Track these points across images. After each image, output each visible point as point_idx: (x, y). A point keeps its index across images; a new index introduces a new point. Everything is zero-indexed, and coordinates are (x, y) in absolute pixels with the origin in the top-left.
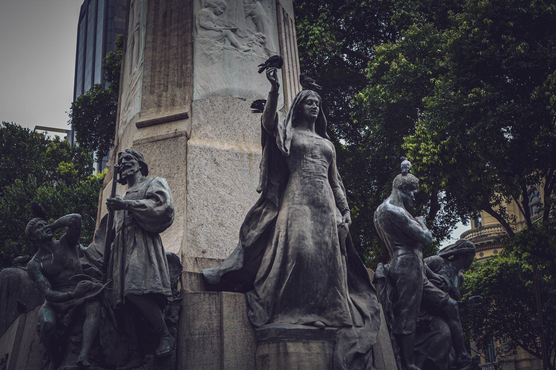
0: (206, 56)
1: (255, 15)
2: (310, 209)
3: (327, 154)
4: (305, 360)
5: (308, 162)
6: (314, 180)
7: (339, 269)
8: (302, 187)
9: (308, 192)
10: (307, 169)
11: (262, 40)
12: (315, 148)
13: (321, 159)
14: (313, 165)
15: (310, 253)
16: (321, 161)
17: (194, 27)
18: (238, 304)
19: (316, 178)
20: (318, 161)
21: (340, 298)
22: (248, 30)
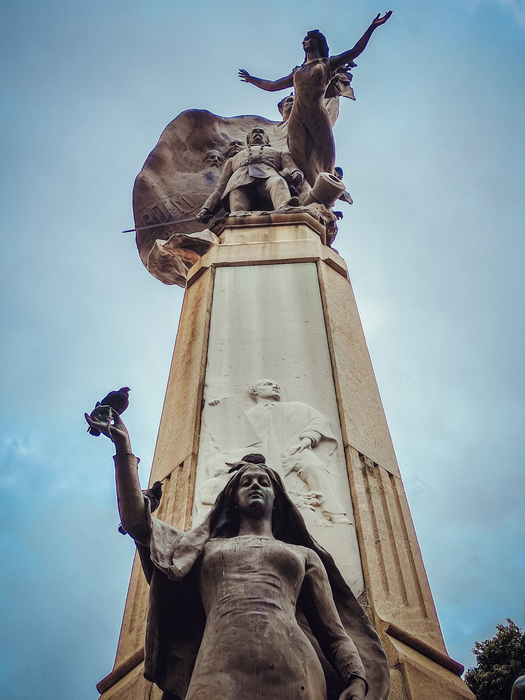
1: (300, 468)
2: (234, 677)
3: (276, 559)
5: (230, 582)
6: (243, 614)
8: (217, 635)
9: (228, 644)
10: (228, 597)
11: (315, 500)
12: (250, 554)
14: (241, 585)
16: (261, 574)
17: (194, 508)
19: (247, 610)
20: (254, 577)
22: (290, 493)
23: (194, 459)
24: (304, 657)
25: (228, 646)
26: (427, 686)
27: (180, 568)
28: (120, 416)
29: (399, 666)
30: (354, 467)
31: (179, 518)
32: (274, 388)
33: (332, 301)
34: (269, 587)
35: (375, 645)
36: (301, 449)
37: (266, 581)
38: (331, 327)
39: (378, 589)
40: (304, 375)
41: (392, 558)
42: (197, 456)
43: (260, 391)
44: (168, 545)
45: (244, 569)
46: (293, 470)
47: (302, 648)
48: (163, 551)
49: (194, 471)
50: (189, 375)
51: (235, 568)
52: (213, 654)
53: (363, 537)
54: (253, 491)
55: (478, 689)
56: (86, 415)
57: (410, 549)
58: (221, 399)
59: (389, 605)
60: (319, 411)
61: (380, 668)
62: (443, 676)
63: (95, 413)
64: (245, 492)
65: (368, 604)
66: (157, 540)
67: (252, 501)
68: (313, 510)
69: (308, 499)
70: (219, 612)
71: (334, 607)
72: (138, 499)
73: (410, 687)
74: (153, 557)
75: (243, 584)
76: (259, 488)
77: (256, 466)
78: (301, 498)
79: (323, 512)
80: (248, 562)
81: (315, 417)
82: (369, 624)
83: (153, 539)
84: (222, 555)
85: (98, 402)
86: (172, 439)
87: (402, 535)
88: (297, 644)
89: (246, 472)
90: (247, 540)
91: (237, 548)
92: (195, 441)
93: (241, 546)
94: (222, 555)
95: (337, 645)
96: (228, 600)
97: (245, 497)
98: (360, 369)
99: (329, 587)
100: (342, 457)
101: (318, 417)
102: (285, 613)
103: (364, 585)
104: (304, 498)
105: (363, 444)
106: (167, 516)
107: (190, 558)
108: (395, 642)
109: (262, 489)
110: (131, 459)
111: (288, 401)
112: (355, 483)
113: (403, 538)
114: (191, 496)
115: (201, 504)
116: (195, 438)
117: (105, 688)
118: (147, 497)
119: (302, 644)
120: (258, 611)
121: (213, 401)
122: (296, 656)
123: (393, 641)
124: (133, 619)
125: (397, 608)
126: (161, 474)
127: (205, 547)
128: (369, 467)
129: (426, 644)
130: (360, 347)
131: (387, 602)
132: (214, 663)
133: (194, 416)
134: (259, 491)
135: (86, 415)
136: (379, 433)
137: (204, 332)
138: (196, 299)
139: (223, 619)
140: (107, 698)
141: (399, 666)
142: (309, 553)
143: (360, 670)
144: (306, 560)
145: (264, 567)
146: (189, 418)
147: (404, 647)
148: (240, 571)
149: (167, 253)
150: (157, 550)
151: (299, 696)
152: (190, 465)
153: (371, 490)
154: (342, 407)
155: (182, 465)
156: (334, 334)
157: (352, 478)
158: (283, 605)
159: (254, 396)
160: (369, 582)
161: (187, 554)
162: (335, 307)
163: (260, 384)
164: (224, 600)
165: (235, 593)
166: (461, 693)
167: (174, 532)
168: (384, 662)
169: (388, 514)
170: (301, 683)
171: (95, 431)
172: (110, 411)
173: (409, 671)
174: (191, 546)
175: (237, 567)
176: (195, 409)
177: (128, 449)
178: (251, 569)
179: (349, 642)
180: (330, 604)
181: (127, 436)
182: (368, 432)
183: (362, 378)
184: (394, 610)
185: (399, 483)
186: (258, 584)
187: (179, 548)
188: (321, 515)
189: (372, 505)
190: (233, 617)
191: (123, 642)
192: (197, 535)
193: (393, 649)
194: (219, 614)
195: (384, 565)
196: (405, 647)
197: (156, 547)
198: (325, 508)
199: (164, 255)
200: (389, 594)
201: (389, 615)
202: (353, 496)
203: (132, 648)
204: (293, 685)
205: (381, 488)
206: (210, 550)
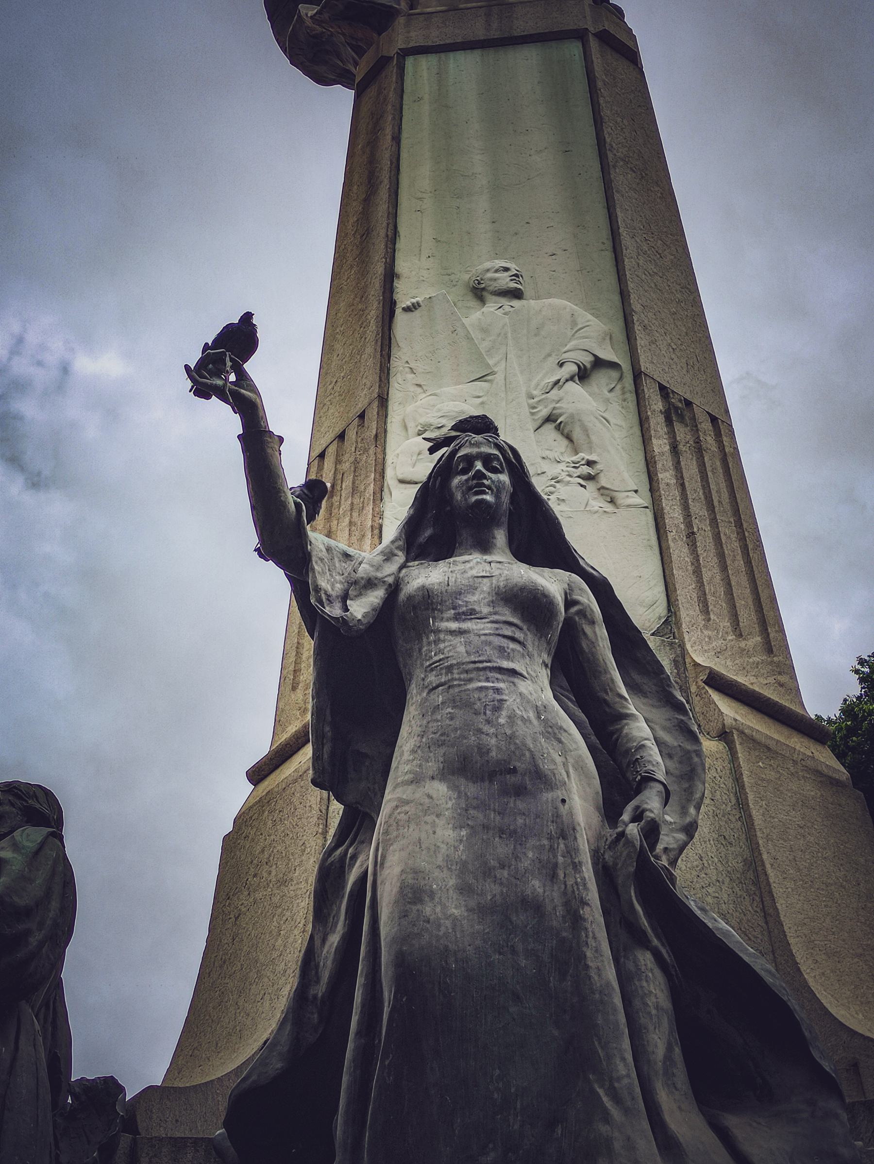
1: (561, 415)
2: (454, 788)
3: (515, 596)
5: (442, 636)
7: (597, 996)
8: (425, 722)
10: (440, 660)
11: (586, 470)
12: (472, 588)
13: (496, 617)
14: (458, 641)
15: (452, 947)
17: (386, 489)
19: (470, 680)
20: (481, 626)
21: (606, 1118)
22: (544, 458)
24: (564, 752)
25: (443, 738)
26: (771, 765)
27: (359, 617)
28: (244, 366)
29: (724, 735)
30: (650, 409)
31: (361, 505)
33: (611, 111)
34: (504, 642)
35: (682, 720)
36: (561, 383)
37: (500, 632)
38: (610, 159)
39: (691, 613)
40: (565, 250)
41: (715, 560)
42: (387, 400)
43: (488, 282)
44: (338, 578)
45: (463, 613)
47: (562, 738)
48: (330, 589)
49: (383, 426)
50: (367, 256)
51: (449, 612)
52: (419, 752)
53: (666, 528)
54: (475, 482)
55: (861, 729)
56: (187, 367)
57: (745, 542)
59: (710, 638)
60: (591, 314)
61: (690, 759)
62: (797, 748)
63: (202, 364)
64: (462, 484)
65: (674, 638)
67: (474, 498)
68: (582, 486)
70: (426, 683)
71: (613, 667)
72: (284, 505)
73: (743, 768)
74: (314, 599)
75: (462, 639)
76: (484, 477)
77: (478, 438)
78: (562, 466)
79: (599, 489)
80: (470, 602)
81: (584, 325)
82: (671, 687)
83: (313, 569)
84: (428, 591)
85: (206, 344)
86: (345, 371)
87: (732, 520)
88: (553, 732)
89: (462, 449)
90: (468, 565)
91: (452, 580)
92: (382, 374)
93: (458, 576)
94: (428, 591)
95: (618, 727)
96: (440, 665)
97: (463, 492)
98: (660, 234)
99: (605, 635)
101: (588, 326)
102: (533, 682)
103: (668, 607)
104: (567, 467)
105: (667, 370)
106: (342, 503)
107: (375, 597)
108: (719, 698)
109: (491, 478)
110: (269, 439)
111: (538, 298)
112: (653, 438)
113: (733, 525)
114: (379, 468)
115: (398, 482)
116: (381, 369)
117: (259, 777)
118: (299, 500)
119: (562, 732)
120: (489, 681)
121: (409, 303)
122: (552, 751)
123: (715, 696)
124: (297, 668)
125: (723, 642)
126: (329, 432)
127: (399, 578)
128: (676, 409)
129: (770, 698)
130: (661, 194)
131: (706, 632)
132: (420, 766)
133: (378, 331)
134: (485, 482)
135: (187, 367)
136: (693, 346)
137: (388, 180)
138: (373, 118)
139: (433, 696)
140: (263, 792)
141: (724, 735)
142: (572, 582)
143: (656, 768)
144: (566, 594)
145: (497, 609)
146: (371, 333)
147: (734, 705)
148: (457, 618)
149: (319, 29)
150: (320, 589)
151: (557, 812)
152: (376, 416)
153: (681, 447)
154: (630, 304)
155: (362, 416)
156: (616, 172)
157: (648, 429)
158: (529, 670)
160: (677, 603)
161: (370, 590)
162: (616, 122)
163: (488, 270)
164: (433, 666)
165: (451, 654)
166: (826, 771)
167: (347, 556)
168: (695, 748)
169: (709, 486)
170: (559, 794)
171: (202, 391)
172: (228, 359)
173: (741, 744)
175: (453, 612)
176: (380, 319)
177: (262, 423)
178: (475, 614)
179: (639, 722)
180: (608, 662)
181: (258, 400)
182: (674, 347)
183: (665, 250)
184: (717, 645)
185: (727, 431)
187: (356, 583)
188: (596, 494)
189: (682, 473)
190: (448, 692)
191: (283, 704)
192: (386, 559)
193: (715, 710)
194: (426, 687)
195: (701, 572)
196: (735, 704)
197: (319, 583)
198: (603, 481)
199: (314, 33)
200: (709, 620)
201: (709, 654)
202: (649, 460)
203: (298, 713)
204: (548, 796)
205: (698, 441)
206: (408, 583)
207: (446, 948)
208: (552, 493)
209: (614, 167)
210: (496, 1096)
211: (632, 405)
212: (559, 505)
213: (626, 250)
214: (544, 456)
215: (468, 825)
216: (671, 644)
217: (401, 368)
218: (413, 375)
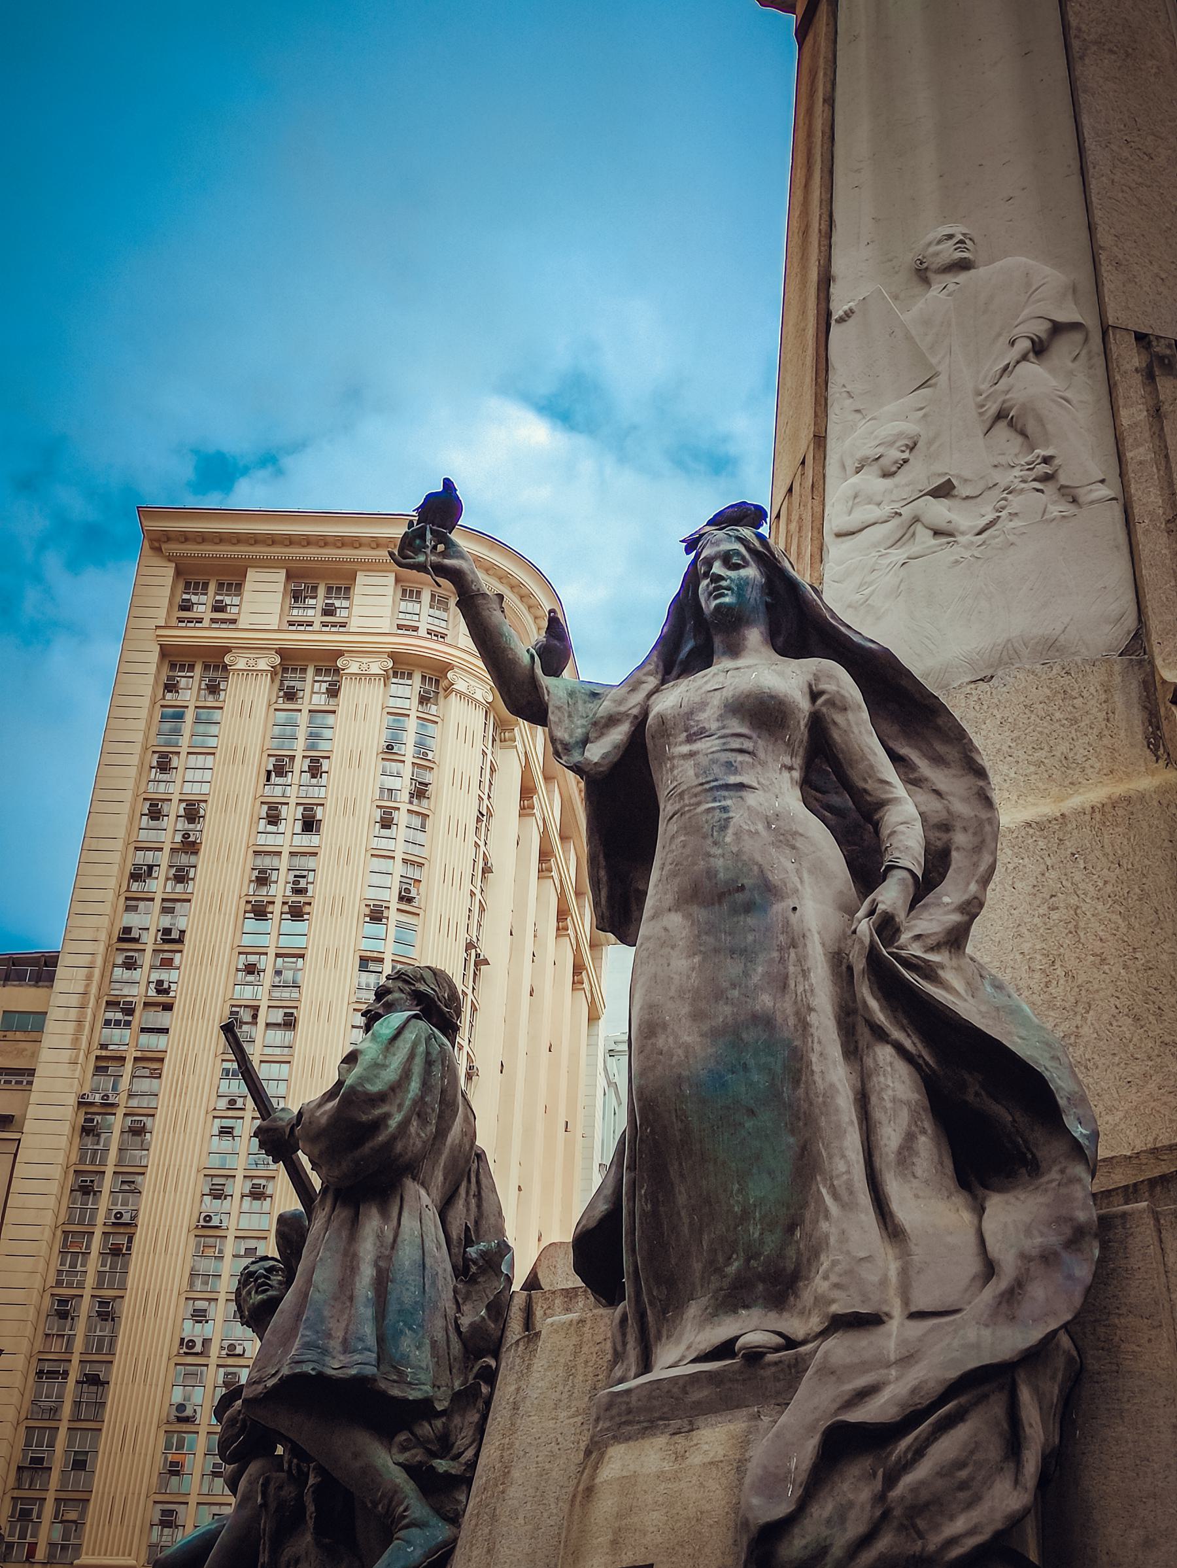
0: (856, 608)
1: (1011, 408)
2: (688, 916)
3: (742, 705)
4: (650, 1501)
11: (1043, 469)
16: (720, 737)
18: (585, 1349)
19: (699, 804)
20: (709, 744)
22: (995, 466)
23: (819, 446)
32: (957, 243)
34: (731, 756)
37: (728, 747)
42: (825, 437)
46: (1000, 416)
58: (856, 302)
66: (555, 723)
68: (1038, 490)
69: (1029, 469)
78: (1017, 472)
100: (1099, 355)
107: (619, 734)
109: (730, 578)
111: (992, 261)
121: (841, 313)
130: (1158, 68)
145: (725, 723)
148: (690, 740)
158: (762, 780)
159: (922, 274)
163: (930, 244)
165: (683, 779)
172: (428, 533)
174: (619, 713)
177: (473, 587)
186: (716, 755)
189: (1165, 441)
198: (1063, 479)
204: (779, 907)
207: (679, 1077)
208: (1003, 508)
209: (1082, 58)
210: (736, 1209)
211: (1101, 372)
212: (1011, 521)
213: (1094, 168)
214: (996, 463)
215: (701, 951)
216: (1140, 662)
217: (838, 395)
218: (851, 400)
